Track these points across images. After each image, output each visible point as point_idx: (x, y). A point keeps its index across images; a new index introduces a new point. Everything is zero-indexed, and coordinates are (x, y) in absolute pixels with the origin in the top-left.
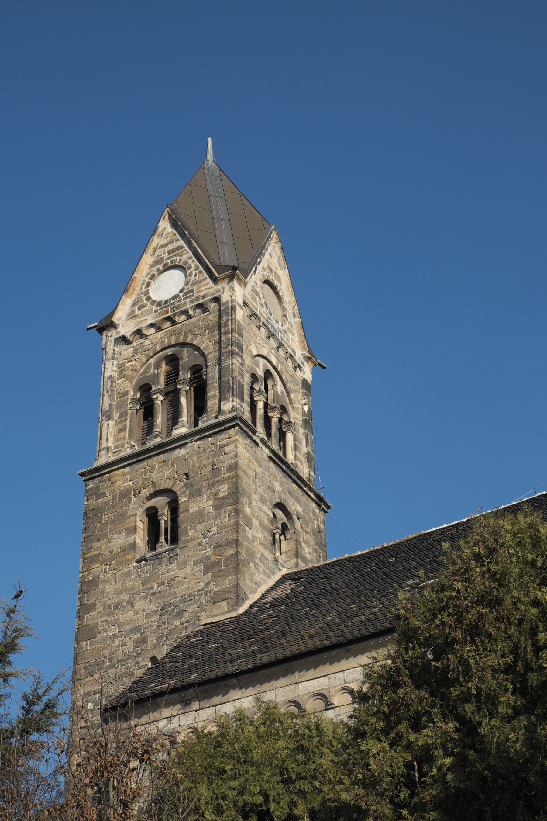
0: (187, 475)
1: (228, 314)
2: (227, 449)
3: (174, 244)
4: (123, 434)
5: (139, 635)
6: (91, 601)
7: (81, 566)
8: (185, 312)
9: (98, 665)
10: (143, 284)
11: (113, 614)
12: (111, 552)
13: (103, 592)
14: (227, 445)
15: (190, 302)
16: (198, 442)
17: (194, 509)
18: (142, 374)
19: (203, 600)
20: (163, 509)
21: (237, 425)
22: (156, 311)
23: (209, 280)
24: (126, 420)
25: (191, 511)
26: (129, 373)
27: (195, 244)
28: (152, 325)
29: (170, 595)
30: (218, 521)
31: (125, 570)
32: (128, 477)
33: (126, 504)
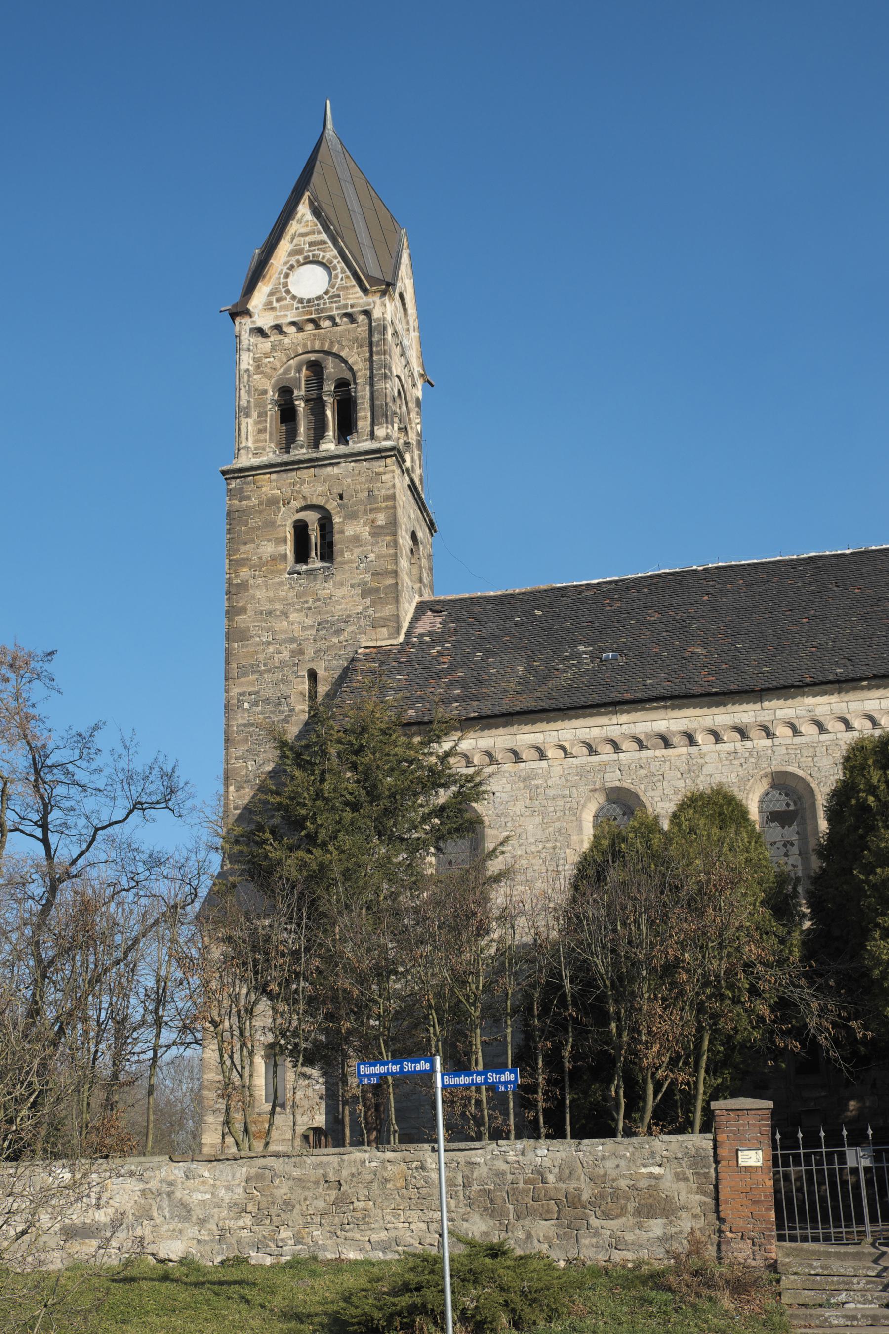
0: (341, 497)
1: (379, 333)
2: (384, 478)
3: (316, 235)
4: (263, 435)
5: (295, 646)
6: (240, 604)
7: (227, 567)
8: (332, 318)
9: (252, 667)
10: (280, 273)
11: (266, 621)
12: (260, 558)
13: (253, 597)
14: (385, 474)
15: (337, 308)
16: (352, 464)
17: (349, 531)
18: (281, 374)
19: (363, 623)
20: (313, 524)
21: (395, 455)
22: (297, 308)
23: (357, 289)
24: (266, 421)
25: (347, 533)
26: (268, 370)
27: (342, 244)
28: (293, 323)
29: (327, 612)
30: (376, 549)
31: (277, 579)
32: (274, 484)
33: (274, 512)
